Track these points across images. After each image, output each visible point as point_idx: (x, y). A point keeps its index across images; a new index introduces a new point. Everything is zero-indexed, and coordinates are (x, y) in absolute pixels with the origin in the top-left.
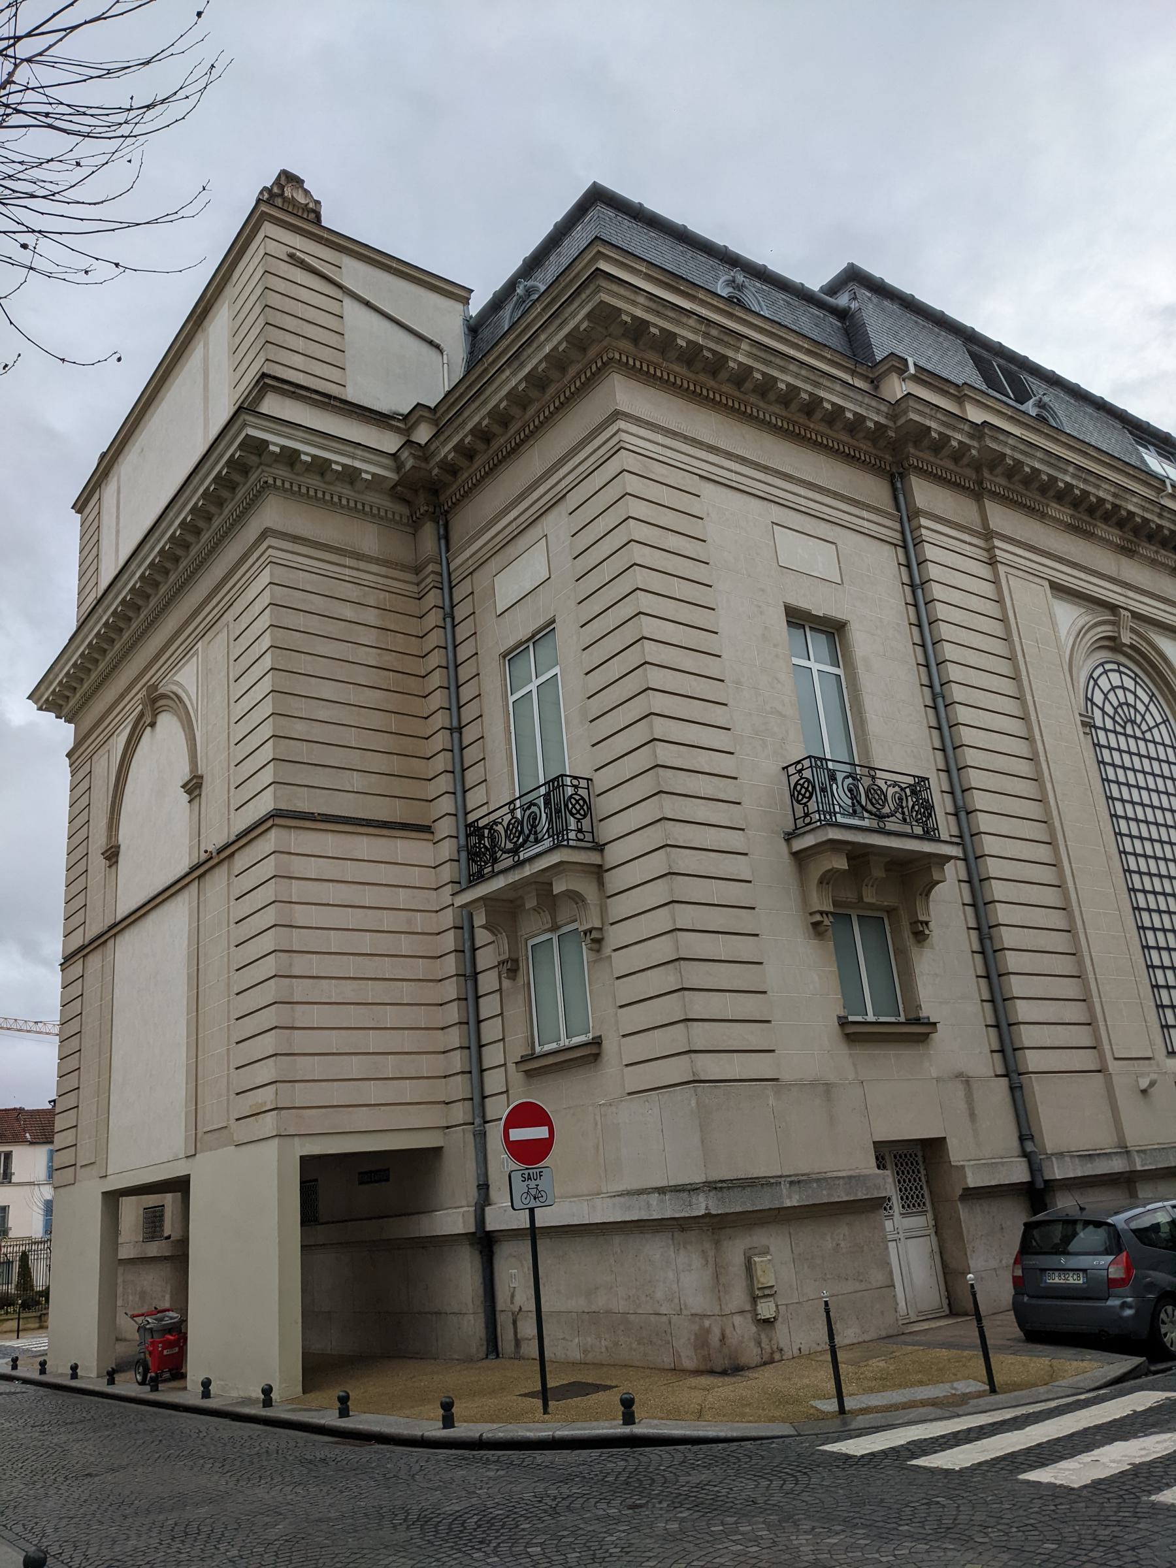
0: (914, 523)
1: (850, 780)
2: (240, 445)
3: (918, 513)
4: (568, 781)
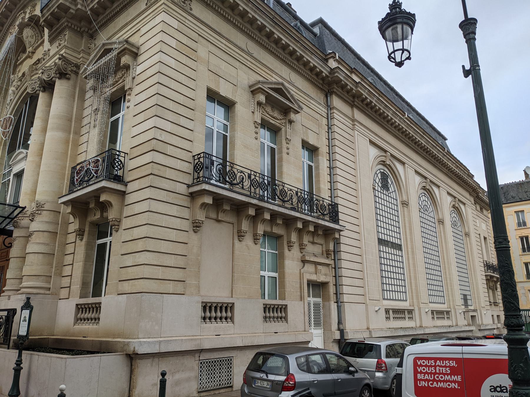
0: (332, 111)
1: (221, 166)
2: (57, 7)
3: (334, 108)
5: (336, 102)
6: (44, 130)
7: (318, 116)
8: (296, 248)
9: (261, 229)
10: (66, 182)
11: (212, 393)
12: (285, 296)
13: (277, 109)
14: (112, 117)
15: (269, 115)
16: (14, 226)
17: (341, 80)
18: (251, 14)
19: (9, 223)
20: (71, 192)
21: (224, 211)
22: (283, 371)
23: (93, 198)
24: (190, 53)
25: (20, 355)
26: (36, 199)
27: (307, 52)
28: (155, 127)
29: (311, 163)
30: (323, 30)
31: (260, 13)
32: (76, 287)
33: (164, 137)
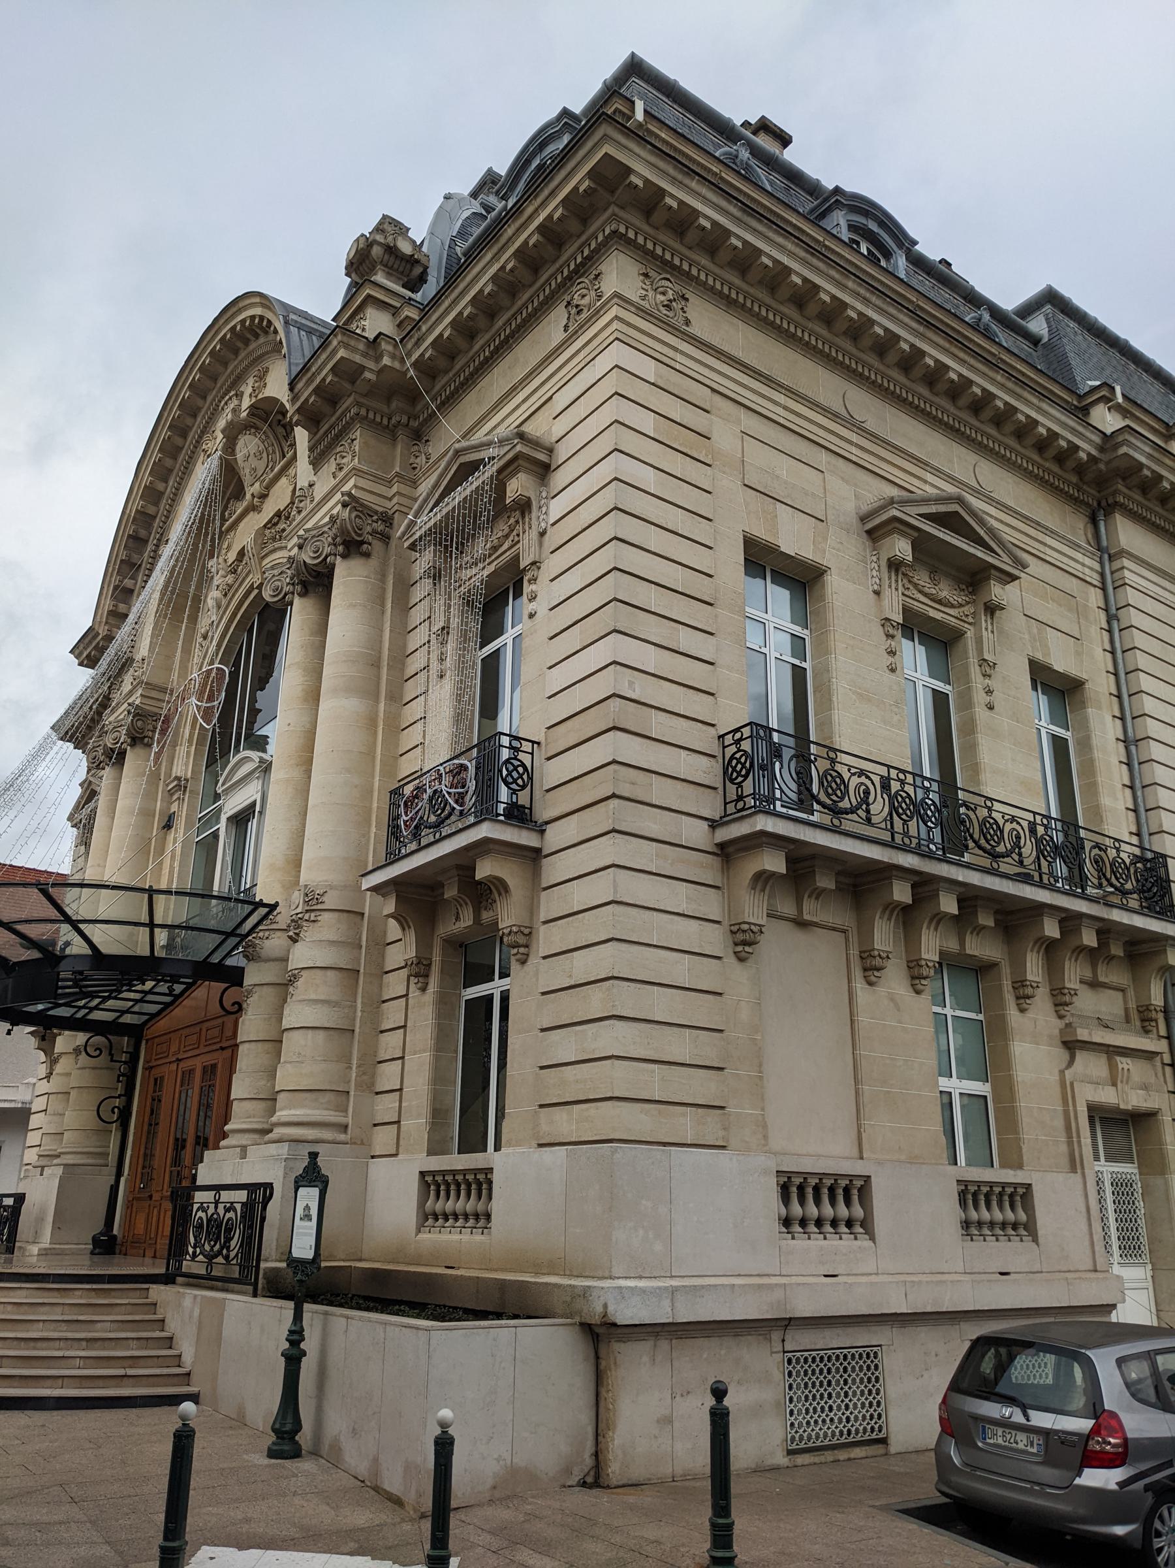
0: (1117, 565)
3: (1122, 553)
4: (505, 741)
5: (1128, 534)
6: (313, 696)
7: (1072, 585)
8: (1042, 1003)
9: (931, 945)
10: (377, 832)
11: (829, 1456)
12: (1021, 1156)
13: (948, 575)
14: (481, 647)
15: (926, 595)
16: (246, 956)
17: (1141, 466)
18: (853, 308)
19: (236, 947)
20: (393, 858)
21: (819, 894)
22: (1079, 1401)
23: (455, 872)
24: (692, 444)
25: (298, 1316)
26: (302, 881)
27: (1026, 395)
28: (615, 662)
29: (1060, 732)
30: (1059, 321)
31: (879, 302)
32: (417, 1124)
33: (642, 689)
